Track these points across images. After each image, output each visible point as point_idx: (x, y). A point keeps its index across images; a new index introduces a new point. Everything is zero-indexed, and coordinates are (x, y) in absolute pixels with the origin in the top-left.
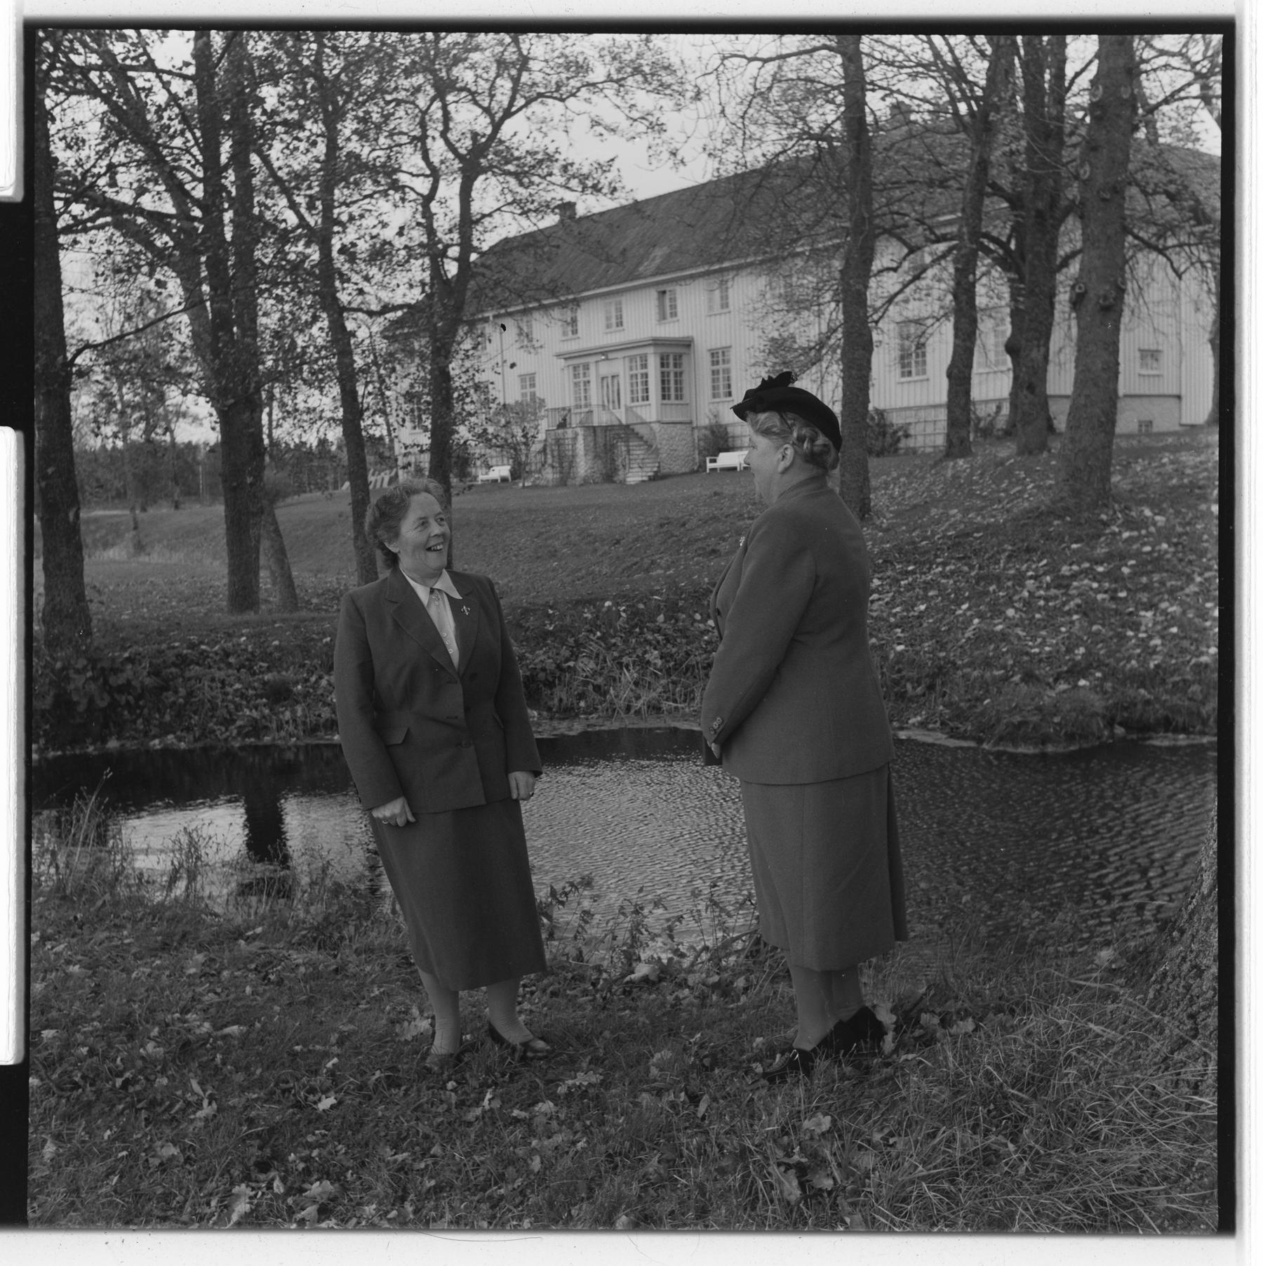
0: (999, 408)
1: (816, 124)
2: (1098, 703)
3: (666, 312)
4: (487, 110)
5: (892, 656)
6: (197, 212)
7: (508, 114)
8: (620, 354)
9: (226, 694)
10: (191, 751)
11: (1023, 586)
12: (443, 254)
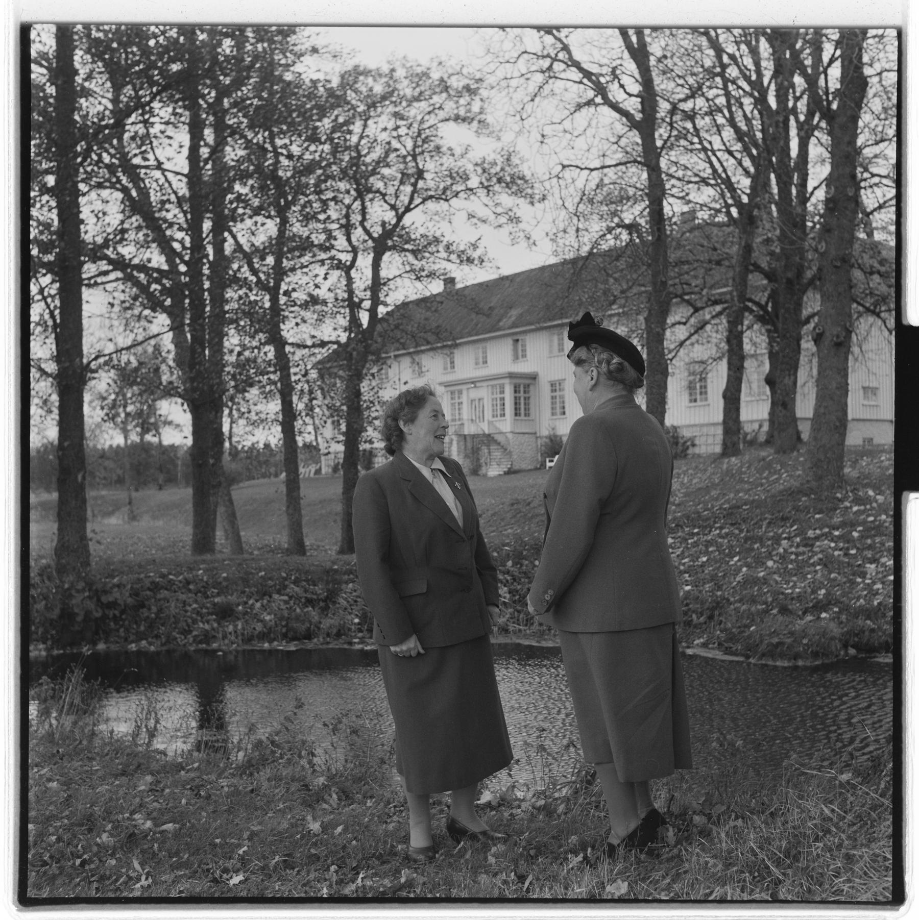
0: (761, 426)
1: (628, 218)
2: (835, 630)
3: (519, 354)
4: (393, 207)
5: (681, 594)
6: (183, 268)
7: (408, 209)
8: (485, 384)
9: (186, 611)
10: (158, 653)
11: (779, 545)
12: (359, 305)
